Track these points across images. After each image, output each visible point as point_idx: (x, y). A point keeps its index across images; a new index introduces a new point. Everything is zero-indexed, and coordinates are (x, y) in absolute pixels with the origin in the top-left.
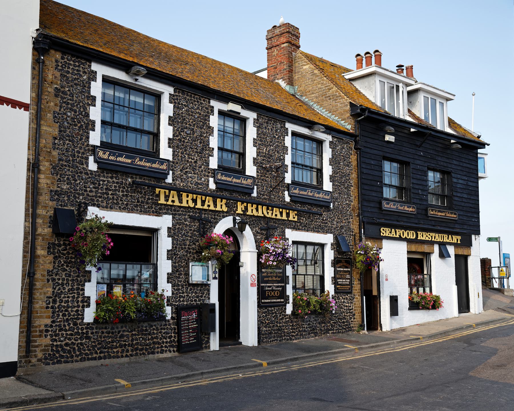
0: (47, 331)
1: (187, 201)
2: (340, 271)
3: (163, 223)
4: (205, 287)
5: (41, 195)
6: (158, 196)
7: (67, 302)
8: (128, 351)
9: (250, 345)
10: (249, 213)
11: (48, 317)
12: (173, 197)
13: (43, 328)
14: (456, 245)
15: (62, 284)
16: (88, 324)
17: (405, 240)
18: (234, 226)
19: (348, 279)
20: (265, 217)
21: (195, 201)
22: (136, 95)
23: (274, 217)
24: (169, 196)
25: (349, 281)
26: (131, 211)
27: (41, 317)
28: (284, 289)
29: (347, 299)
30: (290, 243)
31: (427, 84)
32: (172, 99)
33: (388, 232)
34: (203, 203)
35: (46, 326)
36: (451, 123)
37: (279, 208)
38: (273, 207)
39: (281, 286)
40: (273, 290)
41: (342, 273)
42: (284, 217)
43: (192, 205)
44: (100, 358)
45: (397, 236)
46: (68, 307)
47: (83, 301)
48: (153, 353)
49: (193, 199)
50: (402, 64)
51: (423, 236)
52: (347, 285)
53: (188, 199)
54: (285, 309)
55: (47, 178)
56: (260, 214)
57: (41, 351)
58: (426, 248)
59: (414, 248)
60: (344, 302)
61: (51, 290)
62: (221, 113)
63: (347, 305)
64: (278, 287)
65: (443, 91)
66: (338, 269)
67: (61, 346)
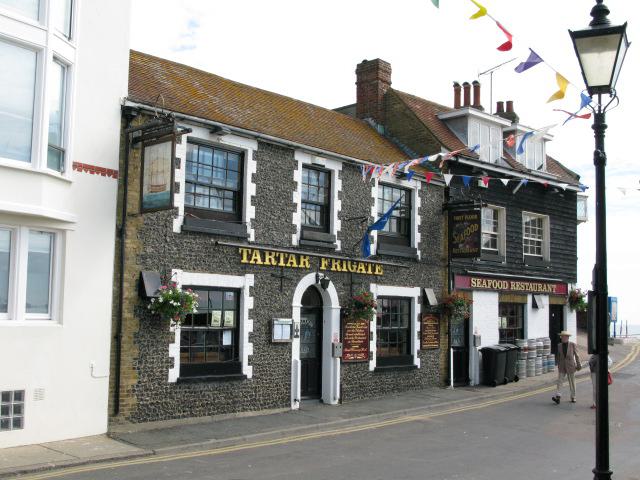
0: (134, 391)
3: (246, 281)
4: (287, 345)
5: (128, 259)
6: (242, 256)
7: (153, 363)
8: (209, 410)
9: (331, 104)
10: (333, 269)
11: (135, 378)
13: (130, 388)
14: (551, 295)
15: (148, 346)
16: (172, 384)
17: (498, 291)
18: (317, 282)
20: (349, 272)
21: (278, 259)
22: (204, 151)
23: (358, 272)
24: (251, 255)
26: (212, 271)
27: (128, 378)
30: (375, 297)
32: (256, 156)
33: (479, 283)
34: (286, 261)
35: (133, 386)
36: (553, 164)
43: (274, 263)
44: (184, 416)
46: (152, 368)
47: (167, 362)
48: (234, 411)
49: (275, 257)
50: (555, 77)
51: (516, 286)
55: (134, 242)
56: (345, 269)
57: (130, 410)
58: (518, 300)
59: (507, 299)
61: (137, 351)
62: (305, 166)
67: (147, 406)
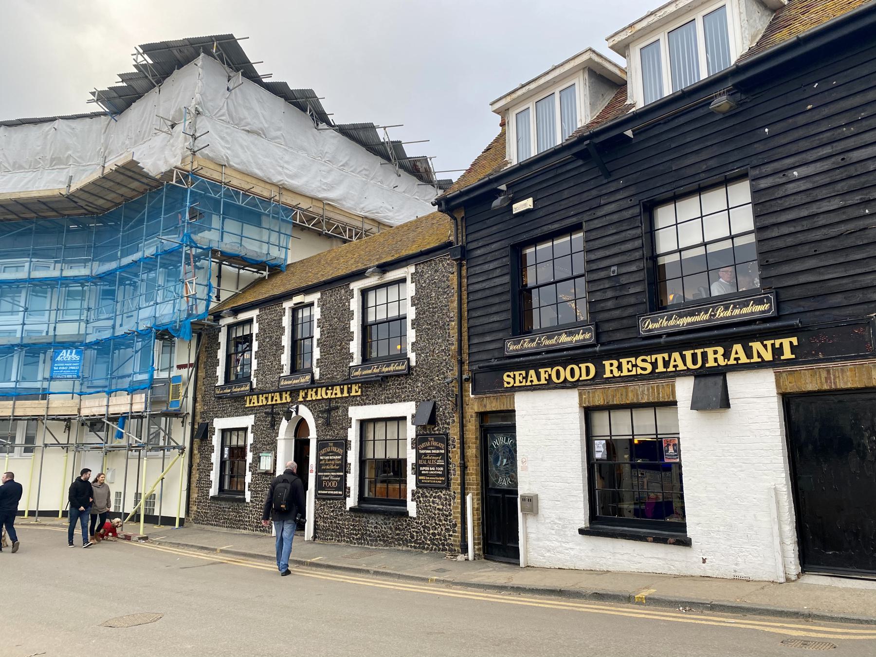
1: (612, 371)
2: (425, 454)
12: (675, 361)
17: (574, 385)
19: (439, 466)
25: (442, 469)
28: (344, 479)
29: (440, 497)
31: (550, 68)
37: (340, 385)
38: (333, 386)
39: (339, 476)
40: (330, 480)
41: (428, 457)
42: (346, 394)
45: (543, 381)
52: (438, 475)
53: (715, 356)
54: (345, 503)
60: (433, 502)
63: (441, 507)
64: (336, 476)
65: (547, 73)
66: (421, 452)
